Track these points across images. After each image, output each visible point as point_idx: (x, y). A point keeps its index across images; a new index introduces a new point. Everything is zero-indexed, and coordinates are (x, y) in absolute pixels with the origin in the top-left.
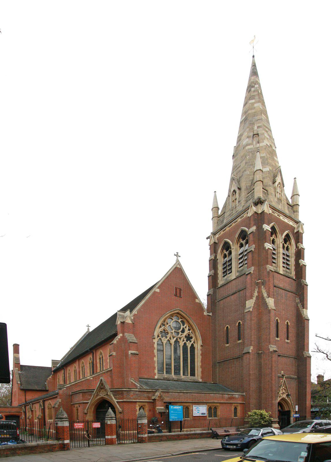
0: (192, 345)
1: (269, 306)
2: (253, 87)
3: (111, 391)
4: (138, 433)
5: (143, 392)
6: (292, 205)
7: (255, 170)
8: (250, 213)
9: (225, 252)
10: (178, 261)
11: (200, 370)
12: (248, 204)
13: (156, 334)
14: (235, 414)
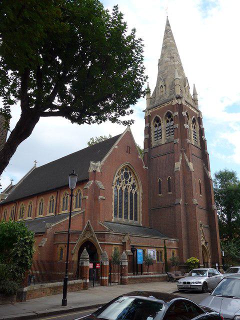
11: (141, 215)
12: (172, 96)
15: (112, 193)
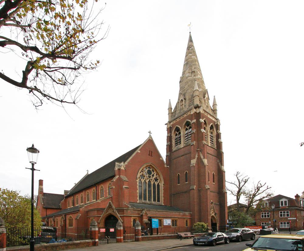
0: (158, 183)
1: (205, 163)
2: (191, 47)
3: (116, 209)
4: (136, 235)
5: (135, 211)
6: (213, 110)
7: (194, 90)
8: (192, 112)
9: (176, 133)
10: (150, 136)
11: (163, 198)
12: (190, 108)
13: (138, 176)
14: (187, 225)
15: (137, 184)
